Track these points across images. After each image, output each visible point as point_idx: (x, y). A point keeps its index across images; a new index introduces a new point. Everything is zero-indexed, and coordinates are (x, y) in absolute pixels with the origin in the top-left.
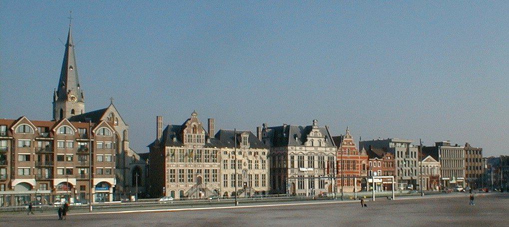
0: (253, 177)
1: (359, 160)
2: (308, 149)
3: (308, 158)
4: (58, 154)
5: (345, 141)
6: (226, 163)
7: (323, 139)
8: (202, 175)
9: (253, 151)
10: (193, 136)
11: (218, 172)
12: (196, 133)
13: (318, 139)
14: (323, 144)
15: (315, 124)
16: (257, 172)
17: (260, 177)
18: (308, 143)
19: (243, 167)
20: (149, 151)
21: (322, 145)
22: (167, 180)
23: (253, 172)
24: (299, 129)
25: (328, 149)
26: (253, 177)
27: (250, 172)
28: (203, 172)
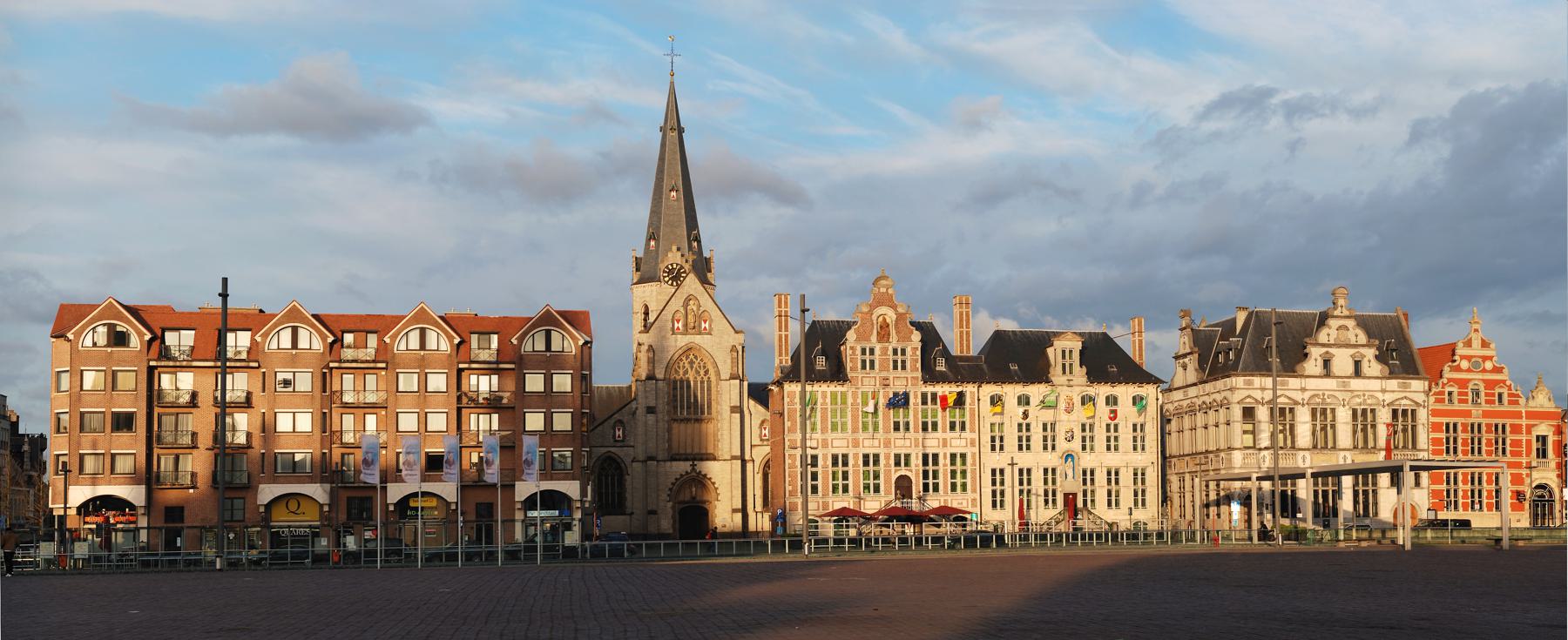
0: (1101, 478)
1: (1524, 422)
2: (1312, 384)
3: (1390, 415)
4: (113, 410)
5: (1462, 357)
6: (1088, 434)
7: (1370, 353)
8: (914, 472)
9: (1103, 391)
10: (877, 352)
11: (969, 460)
12: (888, 341)
13: (1352, 351)
14: (1372, 367)
15: (1341, 302)
16: (1113, 460)
17: (1126, 478)
18: (1312, 366)
19: (1062, 445)
20: (20, 433)
21: (1365, 369)
22: (788, 488)
23: (1098, 460)
24: (779, 371)
25: (1393, 384)
26: (1101, 478)
27: (1087, 461)
28: (916, 461)
